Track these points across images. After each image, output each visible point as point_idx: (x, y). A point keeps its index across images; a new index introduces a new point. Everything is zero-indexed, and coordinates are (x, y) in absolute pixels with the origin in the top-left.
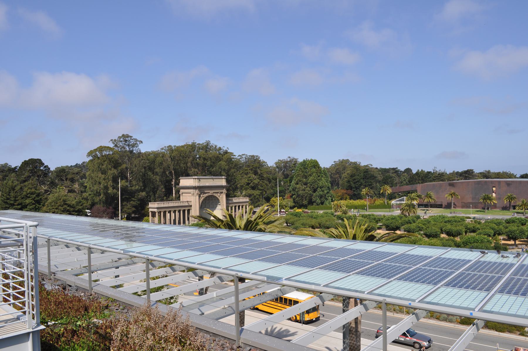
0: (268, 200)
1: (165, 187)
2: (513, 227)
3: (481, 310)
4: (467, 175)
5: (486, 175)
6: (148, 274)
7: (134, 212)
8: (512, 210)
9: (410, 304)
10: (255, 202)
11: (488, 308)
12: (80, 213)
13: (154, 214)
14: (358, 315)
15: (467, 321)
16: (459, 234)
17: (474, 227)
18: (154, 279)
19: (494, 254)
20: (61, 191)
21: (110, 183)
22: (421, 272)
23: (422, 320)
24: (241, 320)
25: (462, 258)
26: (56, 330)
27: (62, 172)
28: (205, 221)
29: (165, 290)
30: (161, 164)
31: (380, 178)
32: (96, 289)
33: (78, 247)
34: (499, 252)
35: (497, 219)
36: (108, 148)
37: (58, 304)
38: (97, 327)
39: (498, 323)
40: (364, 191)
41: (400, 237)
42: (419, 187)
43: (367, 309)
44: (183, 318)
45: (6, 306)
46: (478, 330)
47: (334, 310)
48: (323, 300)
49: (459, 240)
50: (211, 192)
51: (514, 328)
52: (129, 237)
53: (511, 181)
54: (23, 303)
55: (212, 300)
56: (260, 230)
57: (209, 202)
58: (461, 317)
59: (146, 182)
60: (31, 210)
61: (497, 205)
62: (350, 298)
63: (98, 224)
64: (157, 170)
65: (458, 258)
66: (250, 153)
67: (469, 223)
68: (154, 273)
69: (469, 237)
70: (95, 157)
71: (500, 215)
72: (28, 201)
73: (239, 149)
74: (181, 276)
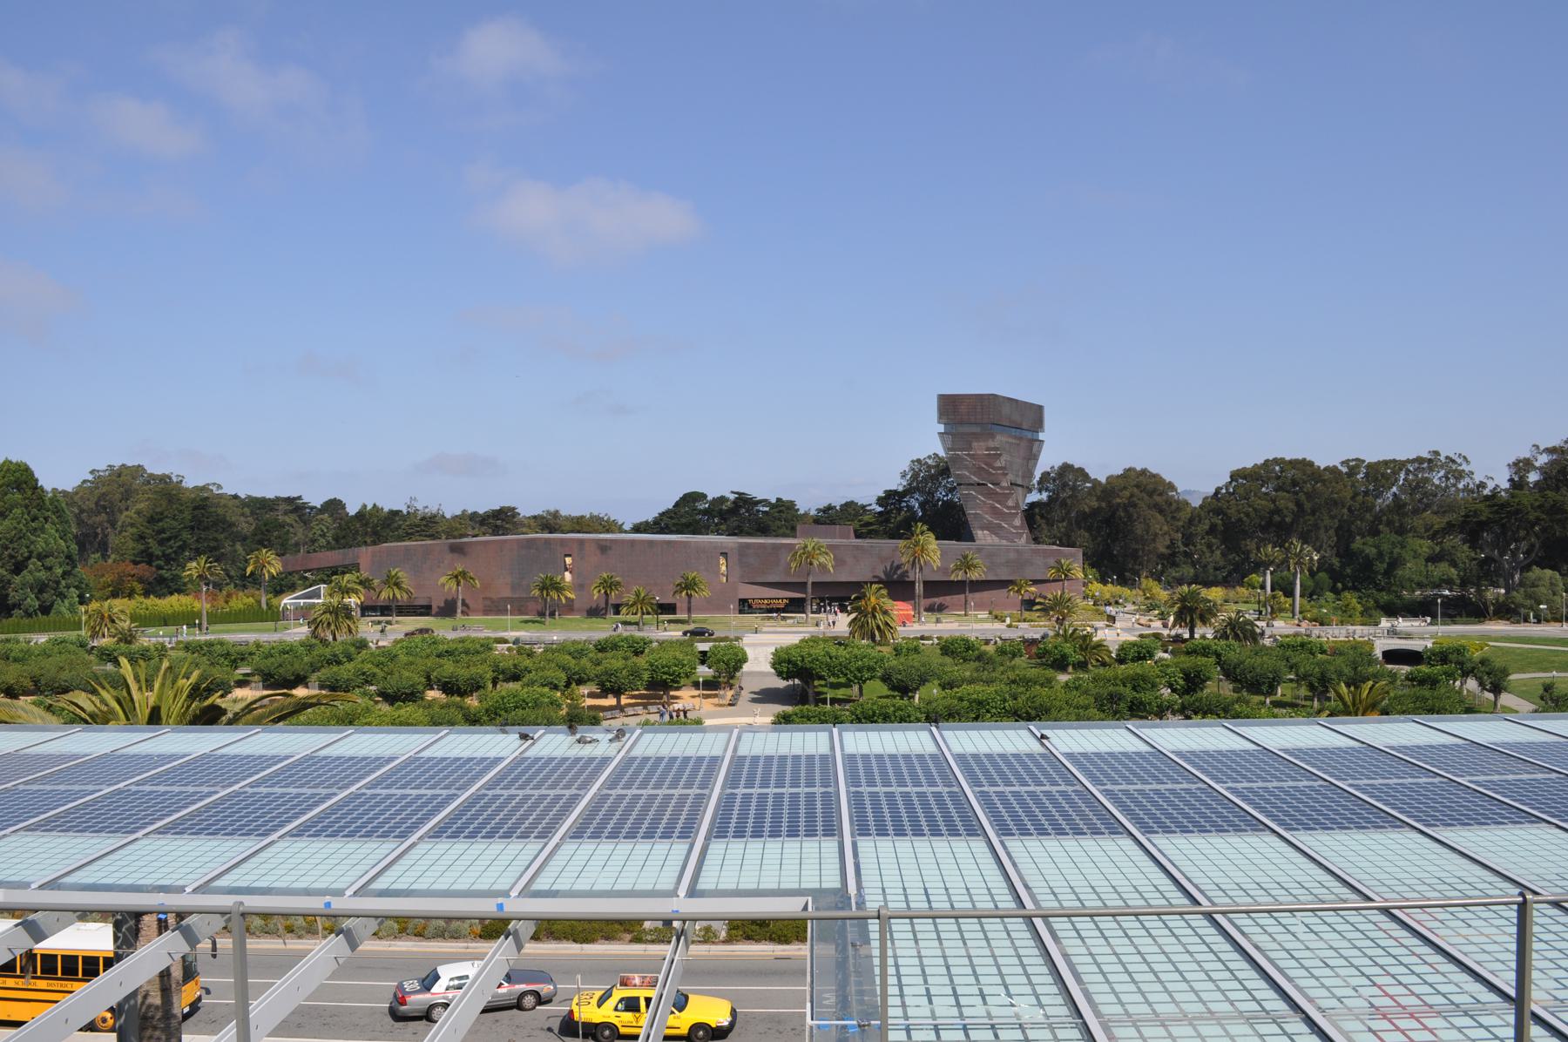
2: (614, 662)
5: (549, 523)
11: (542, 884)
15: (493, 928)
16: (475, 686)
23: (368, 946)
31: (245, 526)
40: (193, 568)
41: (303, 705)
42: (365, 555)
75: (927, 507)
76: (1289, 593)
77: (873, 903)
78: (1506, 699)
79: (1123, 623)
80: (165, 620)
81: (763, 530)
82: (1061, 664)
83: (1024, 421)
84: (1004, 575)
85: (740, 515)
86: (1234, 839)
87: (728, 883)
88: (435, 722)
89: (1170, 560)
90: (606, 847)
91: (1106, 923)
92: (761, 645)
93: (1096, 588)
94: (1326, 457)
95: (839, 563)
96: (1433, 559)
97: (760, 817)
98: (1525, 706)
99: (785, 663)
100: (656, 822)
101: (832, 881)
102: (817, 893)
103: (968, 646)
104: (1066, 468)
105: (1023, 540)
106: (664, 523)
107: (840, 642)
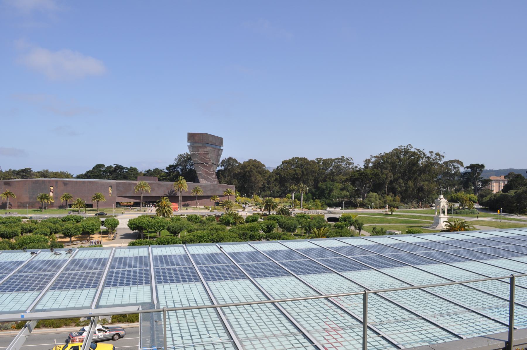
2: (69, 225)
3: (33, 310)
4: (24, 174)
5: (44, 174)
8: (68, 208)
9: (23, 316)
11: (39, 307)
15: (20, 325)
16: (14, 235)
17: (30, 227)
19: (47, 253)
22: (42, 280)
25: (14, 260)
34: (52, 250)
35: (53, 218)
39: (55, 319)
46: (30, 331)
49: (14, 241)
51: (70, 321)
53: (68, 181)
58: (16, 321)
61: (54, 204)
65: (9, 260)
67: (25, 223)
69: (25, 237)
71: (57, 213)
76: (299, 200)
77: (162, 305)
78: (362, 232)
81: (125, 178)
82: (228, 223)
85: (117, 172)
87: (110, 303)
89: (263, 189)
90: (64, 292)
91: (241, 308)
92: (124, 219)
93: (239, 198)
94: (311, 157)
95: (152, 190)
96: (342, 189)
98: (368, 234)
99: (133, 225)
101: (148, 300)
102: (143, 304)
103: (197, 218)
104: (230, 159)
105: (216, 182)
106: (88, 175)
107: (152, 217)
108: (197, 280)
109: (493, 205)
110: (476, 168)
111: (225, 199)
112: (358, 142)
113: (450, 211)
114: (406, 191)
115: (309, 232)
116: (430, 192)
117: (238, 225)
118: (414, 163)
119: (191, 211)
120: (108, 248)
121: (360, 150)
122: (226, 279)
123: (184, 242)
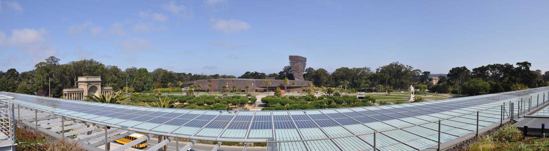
0: (122, 88)
1: (71, 82)
2: (235, 100)
5: (224, 77)
6: (63, 124)
7: (56, 94)
10: (115, 89)
11: (223, 136)
12: (32, 93)
13: (66, 95)
14: (166, 144)
15: (215, 143)
16: (212, 103)
18: (66, 126)
20: (24, 83)
21: (45, 80)
23: (196, 144)
24: (108, 147)
26: (22, 146)
27: (24, 74)
28: (91, 98)
29: (71, 131)
30: (69, 70)
31: (177, 77)
32: (39, 129)
33: (31, 109)
36: (44, 63)
37: (23, 134)
38: (40, 147)
40: (169, 84)
41: (186, 106)
42: (195, 82)
43: (170, 141)
44: (80, 145)
45: (2, 133)
47: (154, 142)
48: (149, 137)
50: (93, 84)
52: (54, 105)
54: (9, 133)
55: (94, 137)
56: (118, 103)
57: (92, 89)
59: (62, 79)
60: (11, 92)
62: (162, 136)
63: (40, 99)
64: (67, 73)
66: (113, 64)
68: (66, 123)
70: (39, 67)
72: (10, 88)
73: (108, 63)
74: (79, 125)
75: (288, 74)
76: (345, 88)
77: (278, 140)
78: (375, 104)
79: (319, 93)
80: (165, 92)
81: (260, 78)
82: (309, 100)
83: (304, 60)
84: (300, 86)
85: (256, 75)
86: (335, 127)
87: (254, 137)
88: (206, 109)
89: (326, 83)
90: (233, 130)
91: (316, 142)
92: (259, 97)
93: (315, 88)
94: (350, 67)
95: (272, 83)
96: (365, 83)
97: (259, 126)
98: (378, 105)
99: (263, 100)
100: (242, 126)
101: (271, 136)
102: (268, 138)
103: (294, 97)
104: (310, 68)
105: (303, 80)
106: (243, 77)
107: (272, 97)
108: (294, 128)
109: (435, 90)
110: (427, 73)
111: (308, 88)
112: (372, 59)
113: (415, 93)
114: (396, 84)
115: (349, 104)
116: (406, 84)
117: (314, 101)
118: (399, 71)
119: (291, 94)
120: (252, 111)
121: (374, 65)
122: (308, 127)
123: (288, 109)
